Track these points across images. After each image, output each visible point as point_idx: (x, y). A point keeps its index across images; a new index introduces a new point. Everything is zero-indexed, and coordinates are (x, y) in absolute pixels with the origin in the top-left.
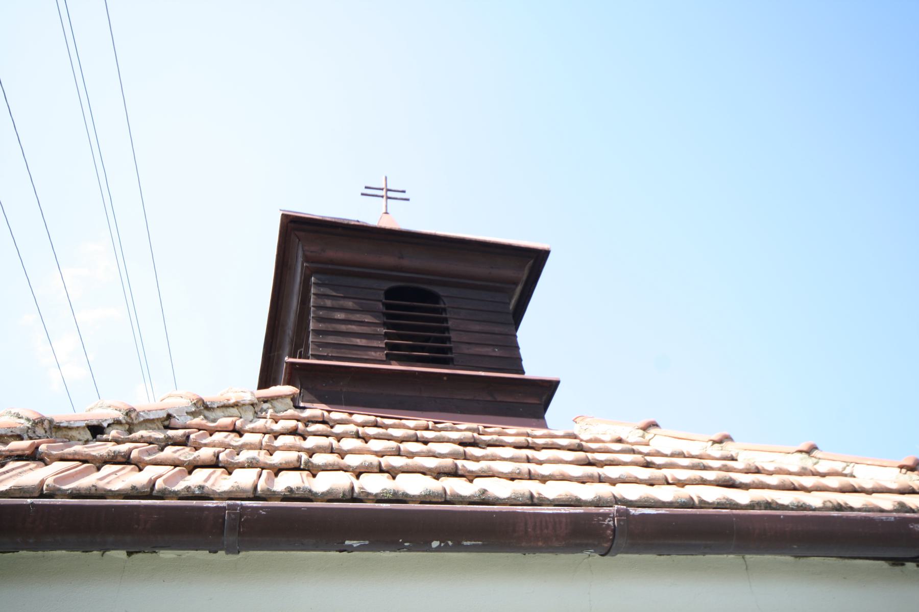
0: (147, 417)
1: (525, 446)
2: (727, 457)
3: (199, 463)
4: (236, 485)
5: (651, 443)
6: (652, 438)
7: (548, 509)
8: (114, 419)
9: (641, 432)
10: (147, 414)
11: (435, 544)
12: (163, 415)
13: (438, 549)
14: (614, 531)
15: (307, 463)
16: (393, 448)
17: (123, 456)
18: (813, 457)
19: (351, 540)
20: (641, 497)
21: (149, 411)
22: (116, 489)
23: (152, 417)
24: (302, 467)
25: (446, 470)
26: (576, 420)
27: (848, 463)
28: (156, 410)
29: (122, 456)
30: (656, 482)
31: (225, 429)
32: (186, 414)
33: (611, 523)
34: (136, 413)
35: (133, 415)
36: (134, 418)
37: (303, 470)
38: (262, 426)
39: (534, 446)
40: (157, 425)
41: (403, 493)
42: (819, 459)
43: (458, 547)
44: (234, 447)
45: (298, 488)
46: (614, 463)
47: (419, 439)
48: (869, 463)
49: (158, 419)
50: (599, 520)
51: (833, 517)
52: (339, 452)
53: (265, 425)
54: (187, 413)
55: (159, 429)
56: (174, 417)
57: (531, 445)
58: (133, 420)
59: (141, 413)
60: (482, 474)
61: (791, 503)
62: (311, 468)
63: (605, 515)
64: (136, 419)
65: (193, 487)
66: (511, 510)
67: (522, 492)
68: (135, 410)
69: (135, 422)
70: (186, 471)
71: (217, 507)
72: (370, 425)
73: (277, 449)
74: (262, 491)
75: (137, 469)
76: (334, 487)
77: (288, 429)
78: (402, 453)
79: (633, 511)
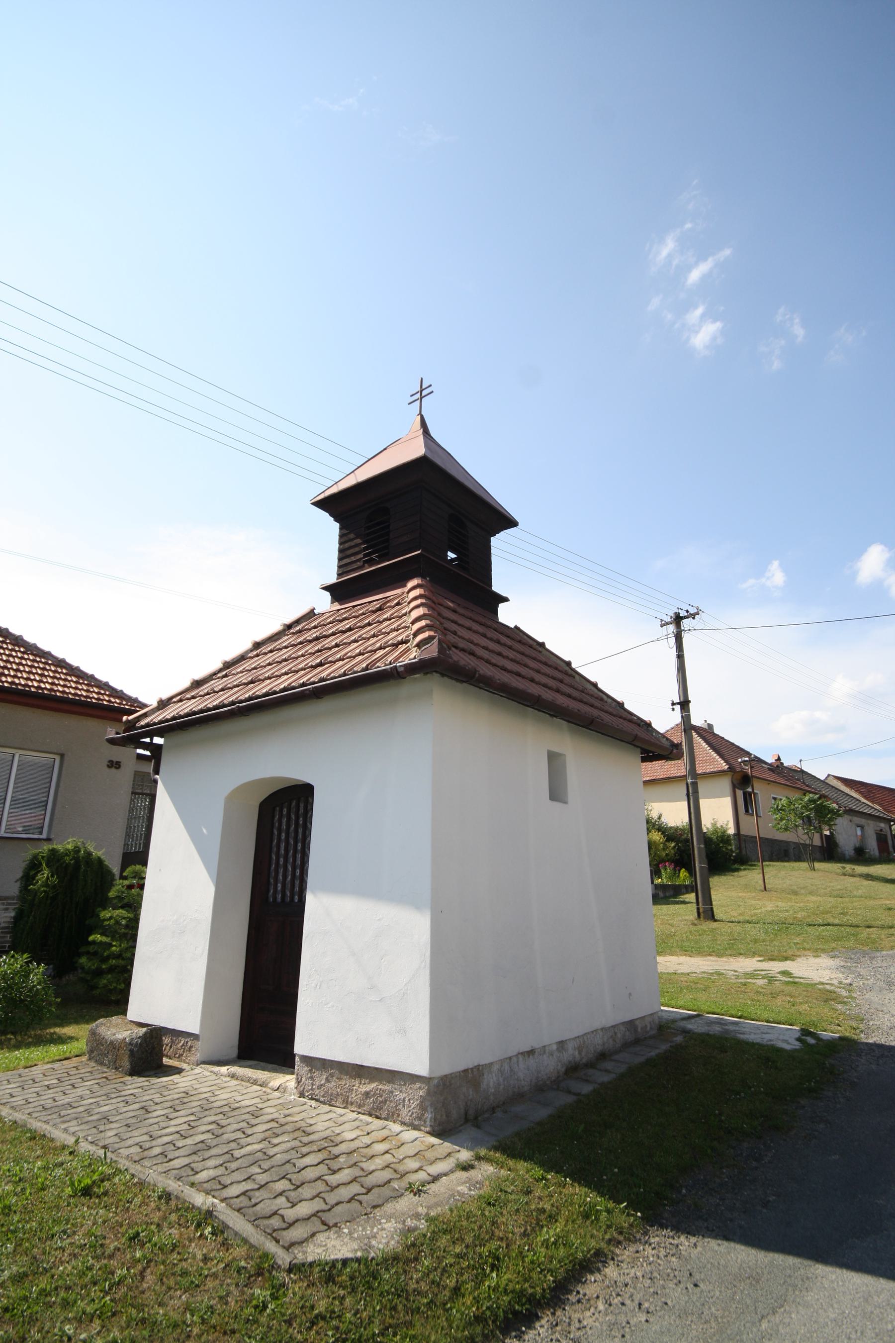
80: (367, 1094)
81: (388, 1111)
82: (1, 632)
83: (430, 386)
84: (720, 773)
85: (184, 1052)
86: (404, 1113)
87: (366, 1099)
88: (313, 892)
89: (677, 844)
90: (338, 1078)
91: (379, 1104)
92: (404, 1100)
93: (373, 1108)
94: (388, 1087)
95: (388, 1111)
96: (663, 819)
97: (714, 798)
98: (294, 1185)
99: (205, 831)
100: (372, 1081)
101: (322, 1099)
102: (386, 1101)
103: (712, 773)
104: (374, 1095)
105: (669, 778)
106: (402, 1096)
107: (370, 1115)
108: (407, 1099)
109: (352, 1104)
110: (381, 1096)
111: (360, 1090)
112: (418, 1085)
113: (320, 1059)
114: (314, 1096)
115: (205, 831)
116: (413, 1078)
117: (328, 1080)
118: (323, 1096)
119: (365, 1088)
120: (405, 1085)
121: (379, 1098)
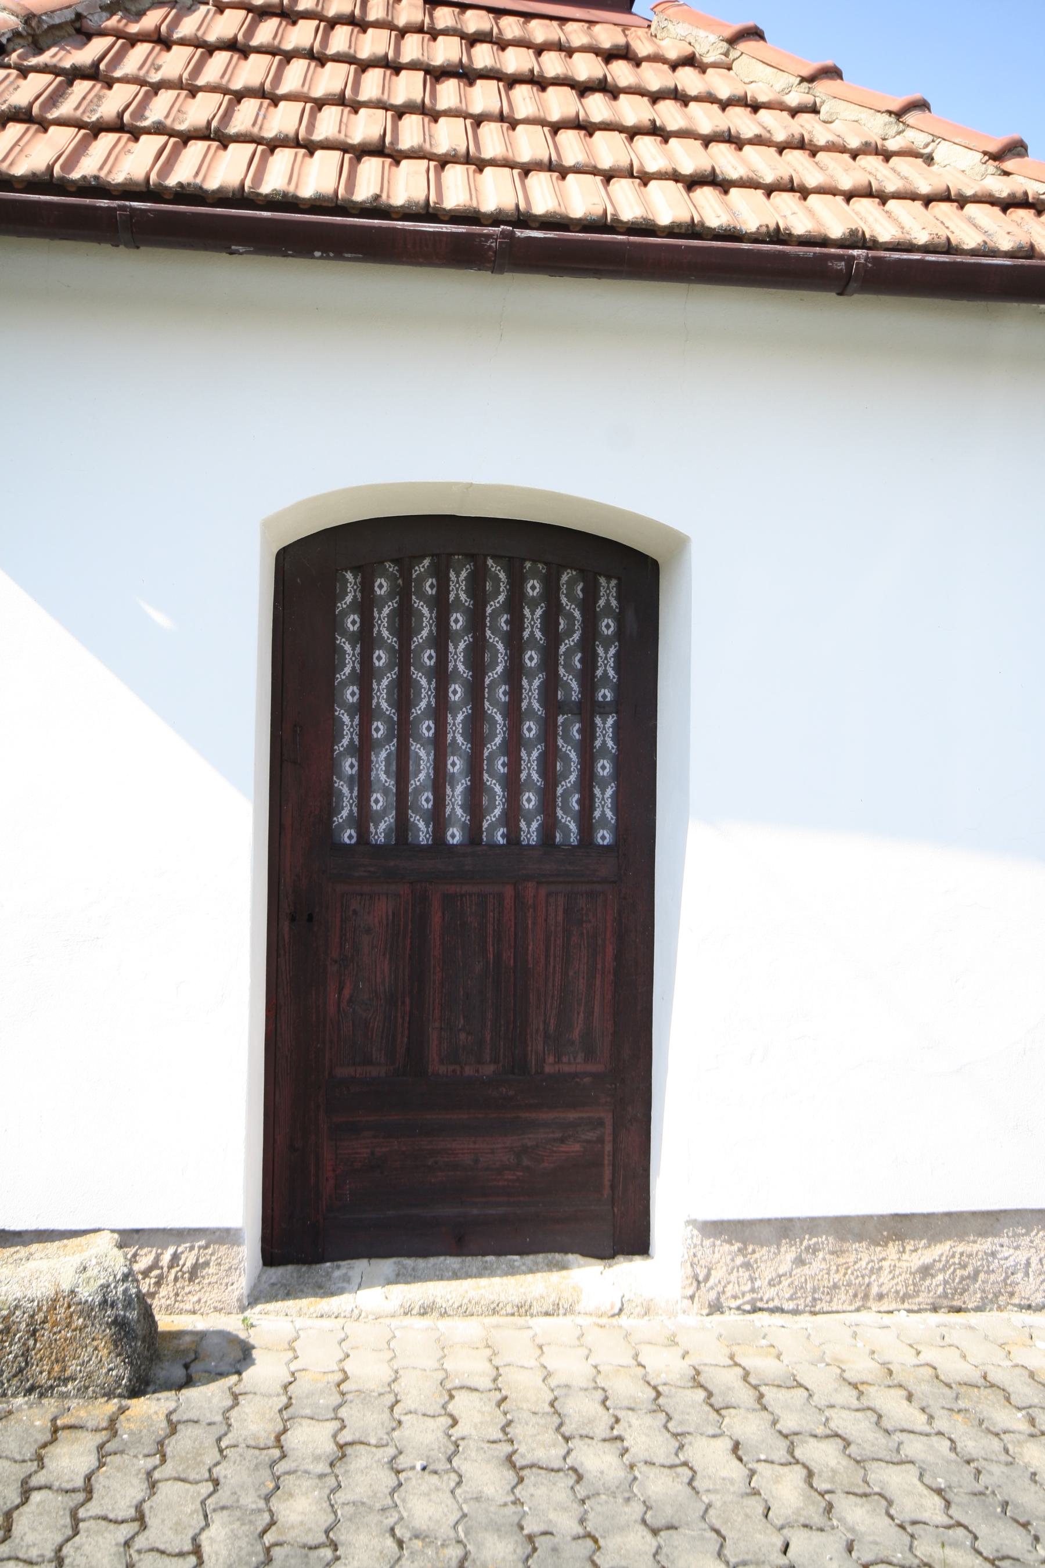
0: (52, 22)
1: (527, 79)
2: (806, 107)
3: (104, 126)
4: (128, 177)
5: (734, 66)
6: (737, 58)
7: (430, 227)
8: (12, 30)
9: (725, 45)
10: (51, 17)
11: (317, 254)
12: (69, 15)
13: (321, 258)
14: (495, 252)
15: (218, 130)
16: (335, 95)
17: (25, 113)
18: (902, 122)
19: (236, 245)
20: (547, 212)
21: (52, 12)
22: (19, 174)
23: (57, 21)
24: (212, 136)
25: (372, 148)
26: (655, 9)
27: (935, 138)
28: (61, 9)
29: (23, 113)
30: (618, 174)
31: (148, 39)
32: (99, 10)
33: (493, 245)
34: (36, 19)
35: (34, 23)
36: (36, 27)
37: (213, 140)
38: (193, 36)
39: (540, 80)
40: (66, 31)
41: (293, 196)
42: (908, 126)
43: (339, 256)
44: (151, 85)
45: (189, 184)
46: (611, 127)
47: (390, 64)
48: (956, 141)
49: (66, 23)
50: (481, 241)
51: (743, 249)
52: (271, 97)
53: (196, 35)
54: (101, 7)
55: (70, 35)
56: (85, 17)
57: (535, 79)
58: (34, 30)
59: (44, 17)
60: (412, 155)
61: (719, 227)
62: (221, 139)
63: (488, 236)
64: (38, 27)
65: (88, 177)
66: (391, 226)
67: (416, 200)
68: (34, 16)
69: (38, 32)
70: (91, 134)
71: (109, 208)
72: (344, 21)
73: (200, 89)
74: (154, 185)
75: (42, 129)
76: (224, 185)
77: (224, 42)
78: (346, 102)
79: (520, 233)
80: (926, 1271)
81: (984, 1291)
82: (3, 1231)
85: (158, 1284)
87: (923, 1279)
90: (832, 1253)
91: (960, 1282)
92: (1028, 1264)
94: (986, 1244)
95: (984, 1291)
98: (951, 1517)
99: (160, 619)
100: (935, 1239)
101: (790, 1306)
102: (977, 1273)
104: (944, 1270)
106: (1022, 1256)
108: (1034, 1261)
109: (881, 1297)
110: (964, 1267)
111: (904, 1264)
113: (769, 1221)
114: (759, 1304)
115: (160, 619)
117: (800, 1262)
118: (791, 1299)
120: (1027, 1234)
121: (959, 1273)
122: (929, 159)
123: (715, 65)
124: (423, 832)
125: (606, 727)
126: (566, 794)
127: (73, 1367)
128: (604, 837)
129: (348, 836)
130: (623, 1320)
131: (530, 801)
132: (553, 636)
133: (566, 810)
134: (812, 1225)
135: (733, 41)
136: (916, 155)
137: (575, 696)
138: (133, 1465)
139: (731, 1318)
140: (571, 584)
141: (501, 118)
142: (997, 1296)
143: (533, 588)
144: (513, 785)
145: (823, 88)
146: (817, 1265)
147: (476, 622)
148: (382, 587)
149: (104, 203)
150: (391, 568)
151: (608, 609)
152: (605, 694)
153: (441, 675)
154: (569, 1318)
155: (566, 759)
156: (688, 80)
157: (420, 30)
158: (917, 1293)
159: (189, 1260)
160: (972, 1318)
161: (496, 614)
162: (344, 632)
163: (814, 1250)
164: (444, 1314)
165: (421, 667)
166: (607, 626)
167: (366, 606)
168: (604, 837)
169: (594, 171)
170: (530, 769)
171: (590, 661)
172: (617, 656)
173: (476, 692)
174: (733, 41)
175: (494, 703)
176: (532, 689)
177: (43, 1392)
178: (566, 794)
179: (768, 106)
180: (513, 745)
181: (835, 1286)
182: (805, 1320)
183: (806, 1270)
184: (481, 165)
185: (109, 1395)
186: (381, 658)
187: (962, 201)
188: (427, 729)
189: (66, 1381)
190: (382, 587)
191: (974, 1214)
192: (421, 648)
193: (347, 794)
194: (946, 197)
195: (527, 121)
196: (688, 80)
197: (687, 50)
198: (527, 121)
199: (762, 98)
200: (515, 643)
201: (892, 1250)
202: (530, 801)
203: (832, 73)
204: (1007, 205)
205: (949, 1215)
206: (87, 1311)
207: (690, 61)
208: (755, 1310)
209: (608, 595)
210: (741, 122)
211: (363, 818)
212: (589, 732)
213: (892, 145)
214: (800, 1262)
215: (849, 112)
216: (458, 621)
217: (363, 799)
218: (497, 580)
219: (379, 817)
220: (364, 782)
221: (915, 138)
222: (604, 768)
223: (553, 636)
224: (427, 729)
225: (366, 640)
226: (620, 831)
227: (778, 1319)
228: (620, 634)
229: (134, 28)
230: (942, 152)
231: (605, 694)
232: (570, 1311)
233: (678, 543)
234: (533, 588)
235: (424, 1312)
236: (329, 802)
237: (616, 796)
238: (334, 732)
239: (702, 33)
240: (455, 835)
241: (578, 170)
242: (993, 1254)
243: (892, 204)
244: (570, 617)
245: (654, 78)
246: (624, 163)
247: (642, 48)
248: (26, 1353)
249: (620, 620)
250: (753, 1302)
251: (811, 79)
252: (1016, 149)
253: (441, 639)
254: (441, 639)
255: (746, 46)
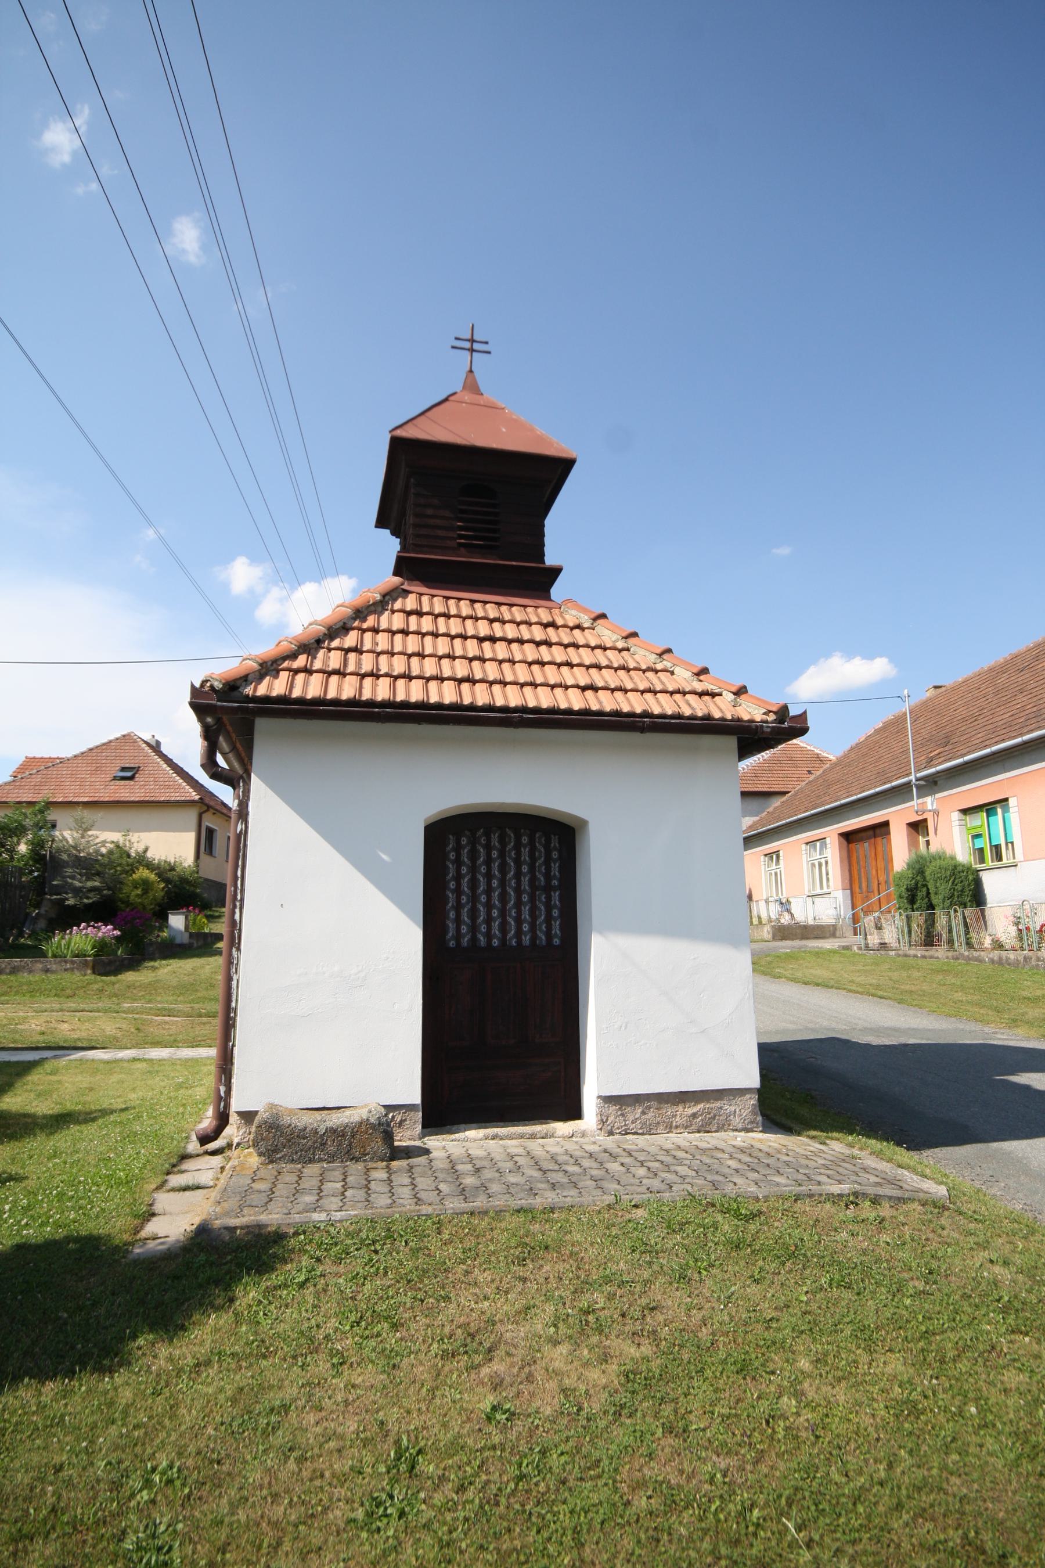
80: (694, 1116)
83: (453, 347)
84: (191, 803)
86: (736, 1122)
88: (600, 932)
89: (166, 886)
93: (702, 1126)
94: (718, 1104)
96: (149, 854)
97: (174, 831)
99: (385, 857)
100: (697, 1102)
101: (641, 1131)
102: (715, 1116)
103: (178, 802)
104: (701, 1115)
105: (118, 802)
106: (733, 1108)
107: (699, 1132)
109: (677, 1127)
112: (748, 1096)
113: (630, 1096)
115: (385, 857)
116: (741, 1092)
117: (643, 1113)
119: (690, 1111)
122: (672, 673)
123: (588, 628)
124: (482, 940)
125: (556, 896)
126: (541, 924)
127: (368, 1149)
128: (556, 941)
129: (452, 944)
130: (574, 1139)
131: (526, 927)
132: (533, 859)
133: (541, 931)
134: (648, 1097)
135: (595, 619)
136: (667, 671)
137: (543, 883)
138: (203, 1434)
139: (617, 1137)
140: (540, 838)
141: (509, 661)
142: (724, 1125)
143: (525, 840)
144: (519, 921)
145: (632, 641)
146: (650, 1115)
147: (502, 854)
148: (464, 841)
149: (377, 710)
150: (467, 833)
151: (555, 848)
152: (555, 882)
153: (489, 876)
154: (552, 1140)
155: (540, 910)
156: (579, 637)
157: (471, 617)
158: (691, 1125)
159: (398, 1119)
160: (714, 1134)
161: (510, 850)
162: (449, 860)
163: (649, 1108)
164: (501, 1139)
165: (480, 873)
166: (555, 855)
167: (458, 849)
168: (556, 941)
169: (547, 685)
170: (526, 914)
171: (548, 869)
172: (560, 867)
173: (503, 883)
174: (595, 619)
175: (510, 887)
176: (525, 881)
177: (357, 1159)
178: (541, 924)
179: (610, 648)
180: (519, 904)
181: (658, 1123)
182: (647, 1137)
183: (646, 1116)
184: (477, 619)
185: (382, 1160)
186: (464, 870)
187: (684, 693)
188: (483, 898)
189: (365, 1155)
190: (464, 841)
191: (713, 1091)
192: (480, 866)
193: (451, 925)
194: (678, 692)
195: (519, 662)
196: (579, 637)
197: (577, 622)
198: (519, 662)
199: (608, 646)
200: (518, 862)
201: (680, 1108)
202: (526, 927)
203: (634, 635)
204: (701, 694)
205: (702, 1091)
206: (373, 1126)
207: (578, 627)
208: (627, 1134)
209: (555, 842)
210: (601, 658)
211: (458, 936)
212: (549, 898)
213: (659, 667)
214: (643, 1113)
215: (641, 652)
216: (495, 854)
217: (458, 929)
218: (510, 837)
219: (464, 936)
220: (458, 921)
221: (667, 664)
222: (555, 913)
223: (533, 859)
224: (483, 898)
225: (458, 862)
226: (562, 939)
227: (635, 1136)
228: (560, 858)
229: (365, 626)
230: (677, 670)
231: (555, 882)
232: (552, 1136)
233: (583, 823)
234: (525, 840)
235: (493, 1138)
236: (445, 929)
237: (560, 924)
238: (446, 900)
239: (582, 615)
240: (495, 943)
241: (542, 685)
242: (721, 1108)
243: (659, 695)
244: (540, 852)
245: (565, 637)
246: (558, 681)
247: (560, 622)
248: (350, 1144)
249: (560, 852)
250: (625, 1130)
251: (626, 638)
252: (705, 671)
253: (489, 861)
254: (489, 861)
255: (600, 621)
